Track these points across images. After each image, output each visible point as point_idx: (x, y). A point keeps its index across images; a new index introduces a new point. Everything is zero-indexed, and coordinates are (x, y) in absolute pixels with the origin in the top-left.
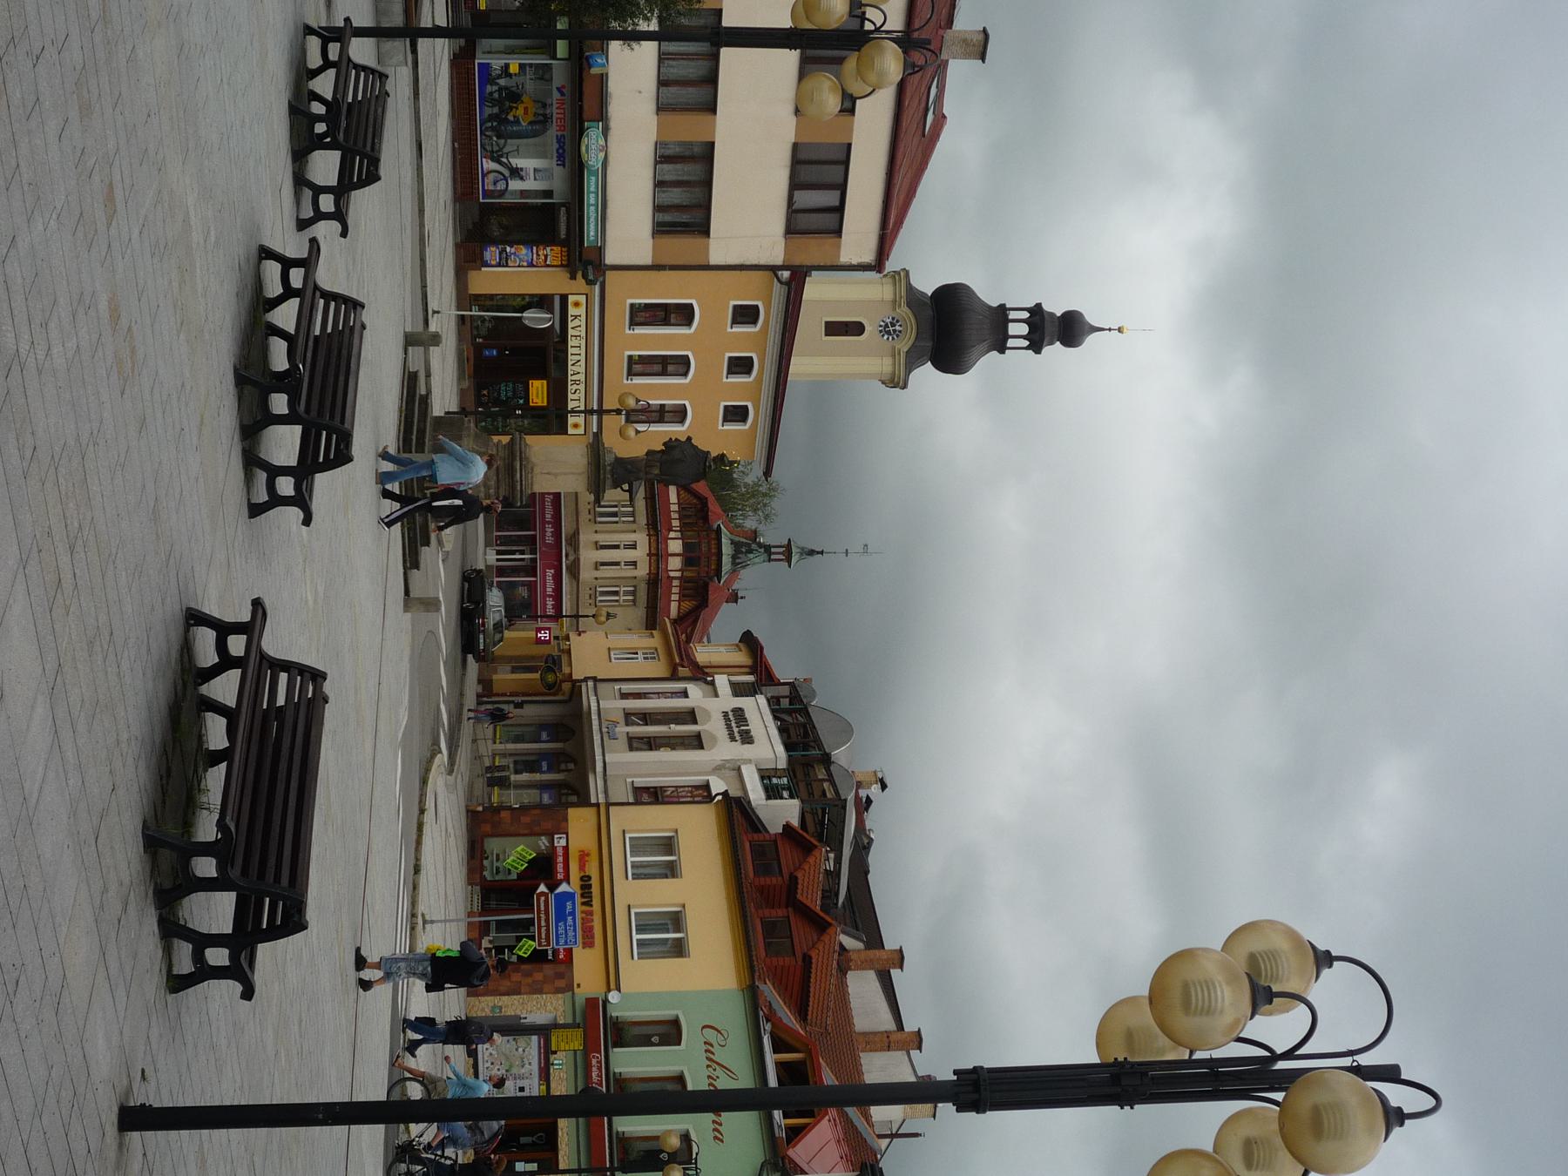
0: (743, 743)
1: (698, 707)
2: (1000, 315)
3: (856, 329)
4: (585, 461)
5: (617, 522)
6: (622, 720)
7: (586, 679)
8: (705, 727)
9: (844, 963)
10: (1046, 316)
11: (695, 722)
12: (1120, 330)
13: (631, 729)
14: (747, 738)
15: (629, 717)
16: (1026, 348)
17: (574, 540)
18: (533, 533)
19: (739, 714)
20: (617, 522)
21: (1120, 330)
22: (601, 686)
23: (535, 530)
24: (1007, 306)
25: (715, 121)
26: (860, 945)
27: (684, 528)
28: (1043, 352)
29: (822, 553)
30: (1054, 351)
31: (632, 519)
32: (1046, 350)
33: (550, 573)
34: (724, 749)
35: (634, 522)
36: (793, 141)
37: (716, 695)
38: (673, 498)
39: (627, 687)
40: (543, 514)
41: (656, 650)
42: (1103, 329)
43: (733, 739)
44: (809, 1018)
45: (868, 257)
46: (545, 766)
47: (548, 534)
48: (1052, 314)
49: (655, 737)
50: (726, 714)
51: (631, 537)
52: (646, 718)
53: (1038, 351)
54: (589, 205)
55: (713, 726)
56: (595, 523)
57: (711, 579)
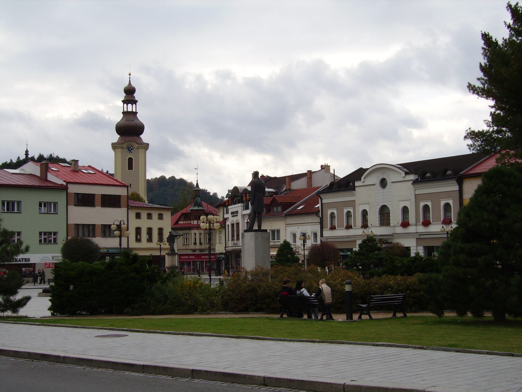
0: (238, 213)
1: (231, 223)
2: (125, 113)
3: (130, 160)
4: (170, 256)
5: (189, 238)
6: (233, 241)
7: (225, 249)
8: (235, 221)
9: (289, 190)
10: (125, 99)
11: (234, 224)
12: (130, 75)
13: (235, 240)
14: (237, 212)
15: (233, 240)
16: (136, 105)
17: (194, 250)
18: (192, 262)
19: (232, 213)
20: (189, 238)
21: (130, 75)
22: (227, 246)
23: (191, 261)
24: (123, 111)
25: (97, 225)
26: (285, 186)
27: (190, 220)
28: (137, 100)
29: (197, 181)
30: (137, 96)
31: (188, 234)
32: (136, 99)
33: (203, 257)
34: (239, 218)
35: (189, 234)
36: (100, 207)
37: (228, 218)
38: (182, 222)
39: (227, 240)
40: (186, 259)
41: (219, 231)
42: (130, 80)
43: (237, 216)
44: (295, 202)
45: (126, 189)
46: (193, 267)
47: (192, 257)
48: (125, 97)
49: (237, 234)
50: (232, 216)
51: (193, 234)
52: (233, 236)
53: (137, 101)
54: (112, 252)
55: (234, 220)
56: (189, 244)
57: (205, 212)
